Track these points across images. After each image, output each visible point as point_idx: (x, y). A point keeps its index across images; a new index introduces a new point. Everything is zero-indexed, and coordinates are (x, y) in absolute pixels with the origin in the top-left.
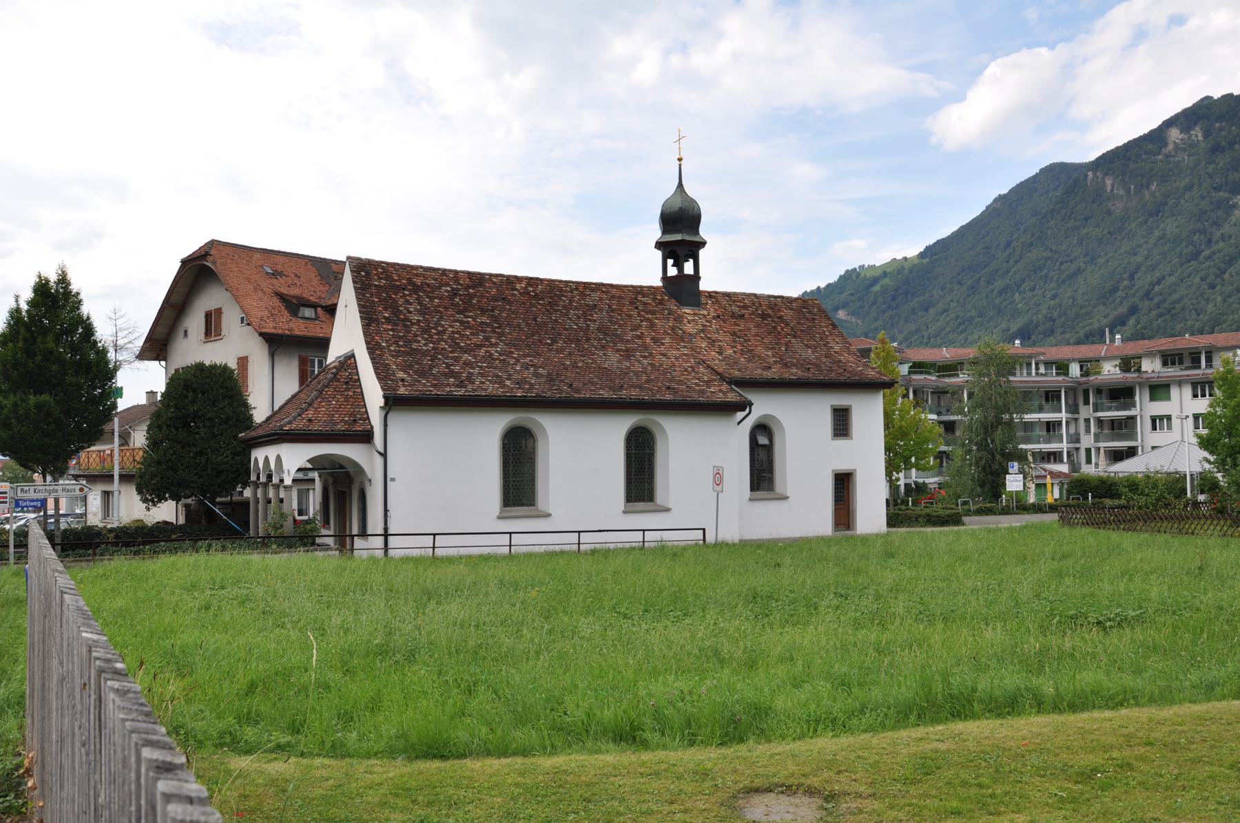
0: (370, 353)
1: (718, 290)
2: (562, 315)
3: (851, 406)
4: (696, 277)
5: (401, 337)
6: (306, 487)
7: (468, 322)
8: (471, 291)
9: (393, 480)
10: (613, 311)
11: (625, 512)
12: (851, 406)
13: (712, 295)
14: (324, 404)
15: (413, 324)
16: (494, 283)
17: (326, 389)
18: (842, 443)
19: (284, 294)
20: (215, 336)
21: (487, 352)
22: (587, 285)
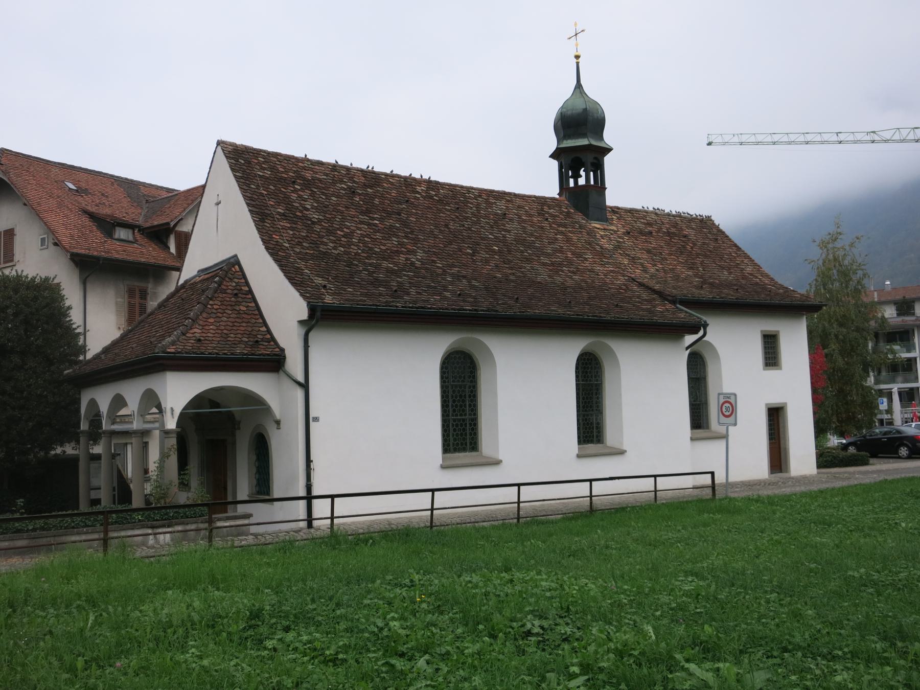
0: (271, 254)
1: (620, 206)
2: (475, 223)
3: (778, 332)
4: (600, 187)
5: (305, 238)
6: (124, 441)
7: (375, 225)
8: (369, 190)
9: (316, 419)
10: (524, 221)
11: (579, 456)
12: (778, 332)
13: (615, 210)
14: (211, 320)
15: (313, 223)
16: (392, 184)
17: (211, 302)
18: (772, 373)
19: (93, 213)
20: (5, 262)
21: (407, 259)
22: (490, 193)
